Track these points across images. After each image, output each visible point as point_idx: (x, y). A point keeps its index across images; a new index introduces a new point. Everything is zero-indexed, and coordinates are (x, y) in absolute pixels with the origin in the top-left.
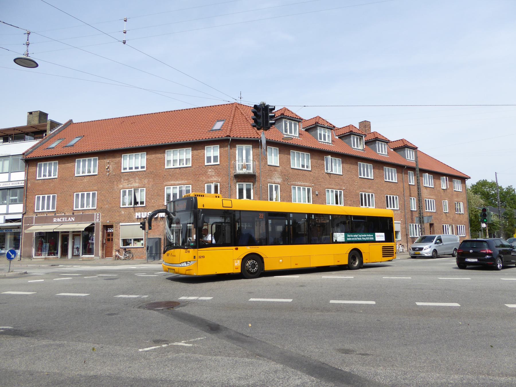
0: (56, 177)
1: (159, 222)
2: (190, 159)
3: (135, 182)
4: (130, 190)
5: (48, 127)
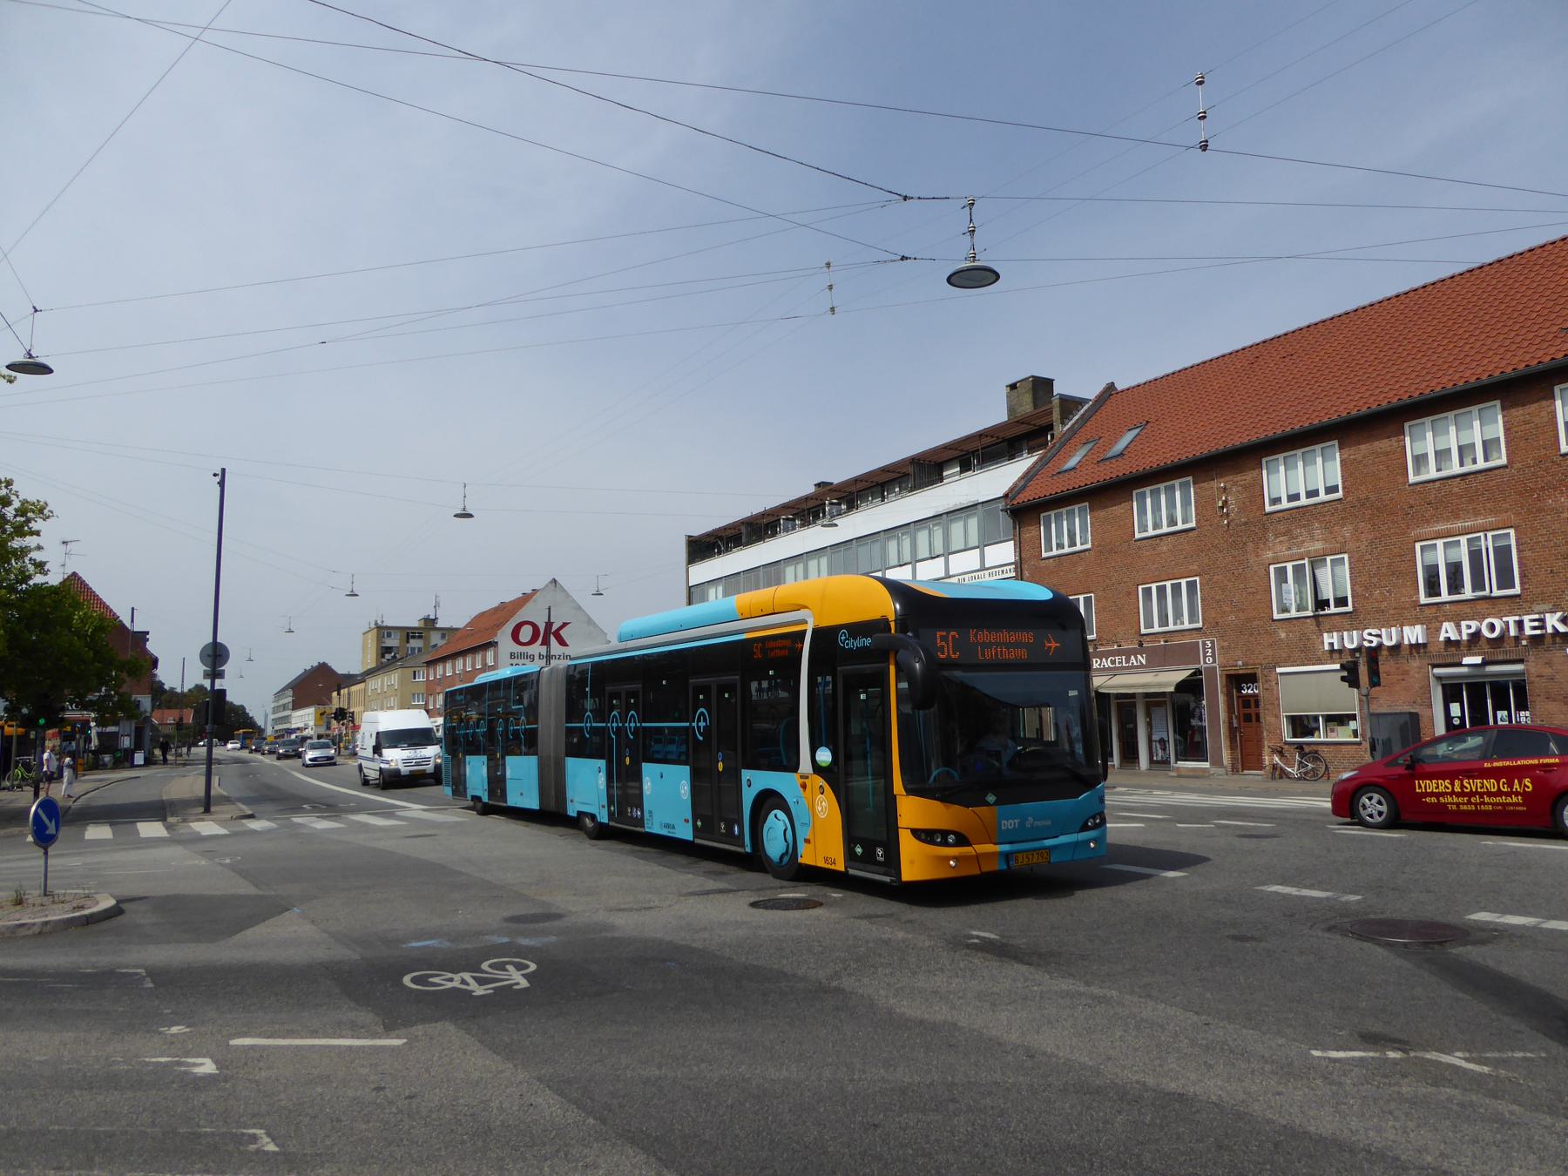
0: (1089, 546)
1: (1404, 661)
2: (1449, 450)
3: (1312, 538)
4: (1496, 535)
5: (1056, 415)
